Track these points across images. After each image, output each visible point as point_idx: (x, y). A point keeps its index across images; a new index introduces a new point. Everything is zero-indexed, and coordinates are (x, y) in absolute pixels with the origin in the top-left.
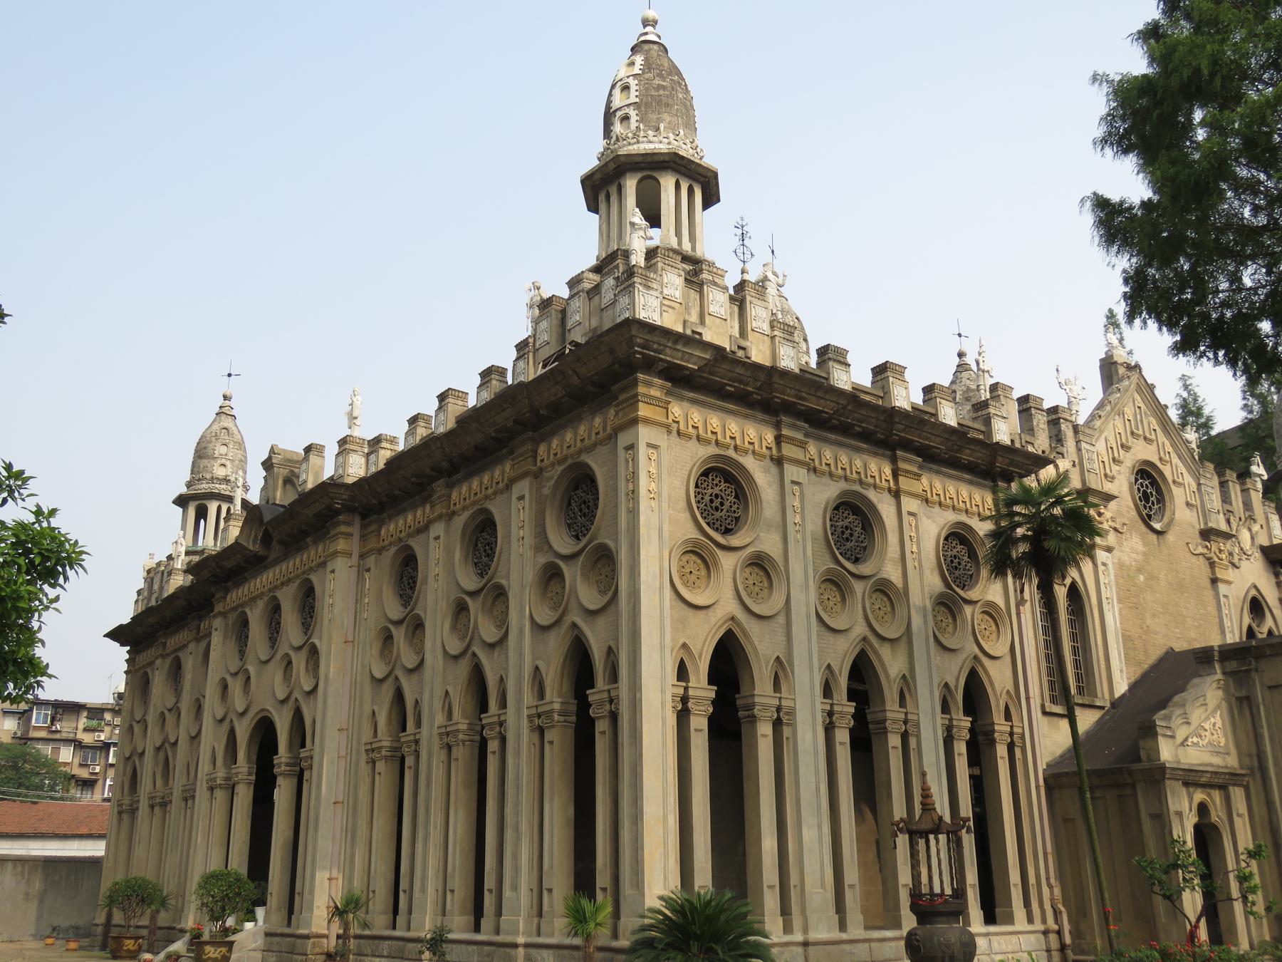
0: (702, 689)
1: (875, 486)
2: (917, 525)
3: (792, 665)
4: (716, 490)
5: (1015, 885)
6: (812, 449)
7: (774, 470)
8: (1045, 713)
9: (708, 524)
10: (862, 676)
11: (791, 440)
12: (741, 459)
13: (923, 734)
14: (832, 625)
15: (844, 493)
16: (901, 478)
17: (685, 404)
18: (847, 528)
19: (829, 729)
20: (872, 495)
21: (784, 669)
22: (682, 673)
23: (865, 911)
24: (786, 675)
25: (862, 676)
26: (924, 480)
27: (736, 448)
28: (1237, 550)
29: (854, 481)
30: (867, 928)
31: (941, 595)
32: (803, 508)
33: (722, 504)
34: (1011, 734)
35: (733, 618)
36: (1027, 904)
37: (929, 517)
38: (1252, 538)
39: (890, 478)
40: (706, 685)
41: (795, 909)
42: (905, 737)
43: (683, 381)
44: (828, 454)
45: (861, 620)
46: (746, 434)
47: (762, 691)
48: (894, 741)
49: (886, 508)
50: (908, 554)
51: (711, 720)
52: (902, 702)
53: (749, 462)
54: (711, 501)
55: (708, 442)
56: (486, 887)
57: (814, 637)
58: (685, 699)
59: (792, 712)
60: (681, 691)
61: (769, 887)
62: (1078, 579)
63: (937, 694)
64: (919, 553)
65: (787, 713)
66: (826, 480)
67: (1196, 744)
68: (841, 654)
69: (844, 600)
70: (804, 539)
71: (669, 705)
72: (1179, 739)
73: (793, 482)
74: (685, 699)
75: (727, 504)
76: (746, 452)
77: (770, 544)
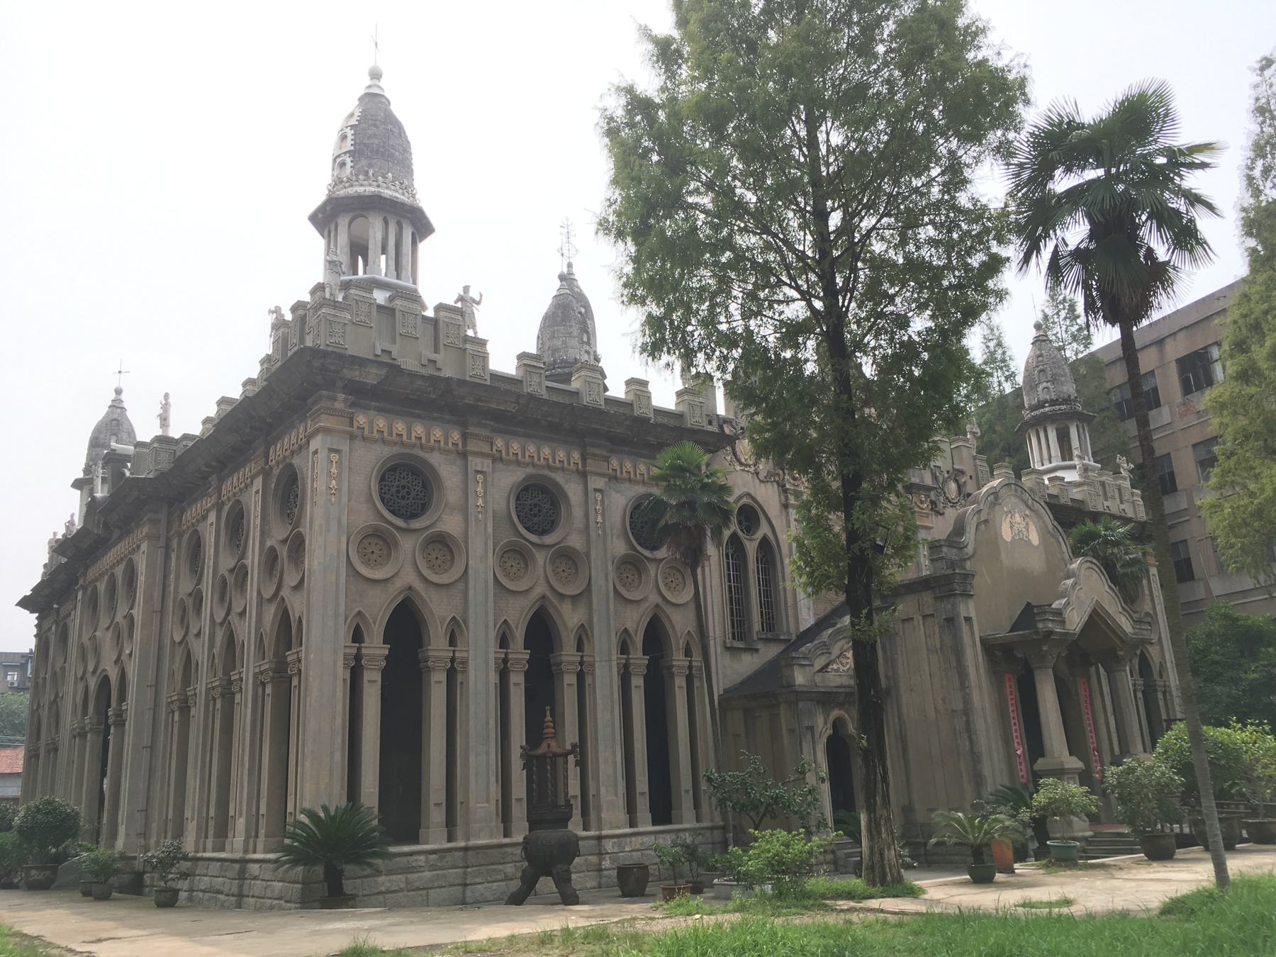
0: (520, 653)
1: (563, 469)
2: (602, 500)
3: (465, 622)
4: (403, 482)
5: (642, 794)
6: (499, 443)
7: (459, 462)
8: (727, 649)
9: (527, 529)
10: (541, 631)
11: (477, 437)
12: (553, 475)
13: (598, 672)
14: (674, 601)
15: (527, 478)
16: (589, 461)
17: (372, 413)
18: (535, 505)
19: (504, 675)
20: (559, 477)
21: (460, 626)
22: (504, 642)
23: (652, 809)
24: (462, 632)
25: (541, 631)
26: (615, 463)
27: (421, 446)
28: (942, 499)
29: (543, 467)
30: (654, 823)
31: (626, 556)
32: (485, 493)
33: (408, 493)
34: (690, 668)
35: (410, 588)
36: (697, 805)
37: (618, 492)
38: (959, 487)
39: (580, 462)
40: (350, 644)
41: (459, 821)
42: (581, 677)
43: (362, 395)
44: (516, 446)
45: (542, 581)
46: (429, 437)
47: (437, 646)
48: (570, 680)
49: (573, 490)
50: (592, 524)
51: (385, 673)
52: (580, 648)
53: (435, 459)
54: (398, 492)
55: (637, 482)
56: (514, 797)
57: (612, 606)
58: (358, 657)
59: (465, 662)
60: (354, 651)
61: (517, 800)
62: (770, 535)
63: (614, 640)
64: (603, 523)
65: (462, 663)
66: (627, 484)
67: (837, 670)
68: (518, 614)
69: (527, 566)
70: (486, 518)
71: (340, 663)
72: (818, 666)
73: (477, 472)
74: (358, 657)
75: (413, 493)
76: (433, 449)
77: (450, 524)
